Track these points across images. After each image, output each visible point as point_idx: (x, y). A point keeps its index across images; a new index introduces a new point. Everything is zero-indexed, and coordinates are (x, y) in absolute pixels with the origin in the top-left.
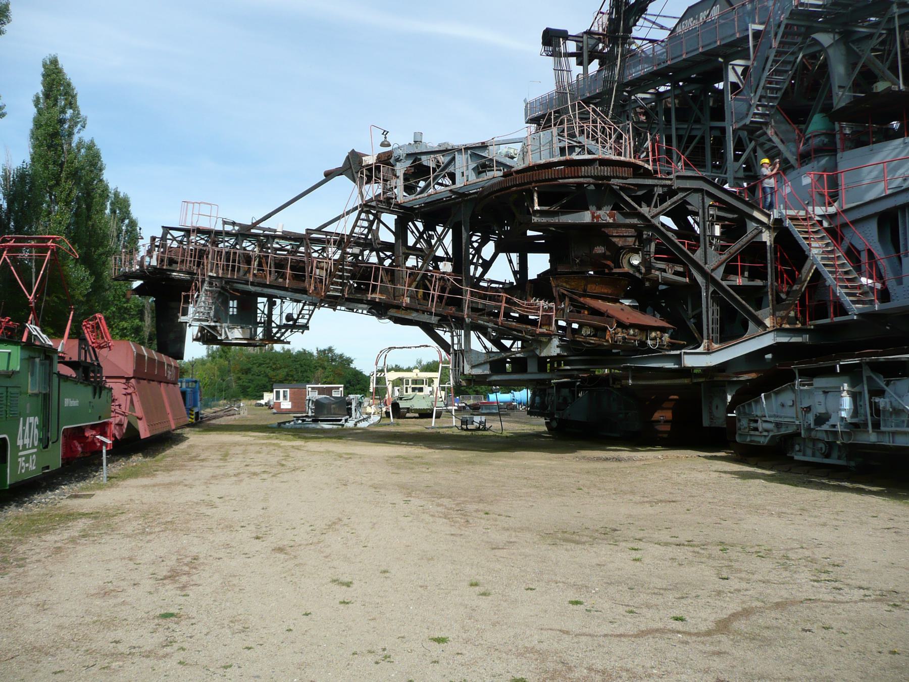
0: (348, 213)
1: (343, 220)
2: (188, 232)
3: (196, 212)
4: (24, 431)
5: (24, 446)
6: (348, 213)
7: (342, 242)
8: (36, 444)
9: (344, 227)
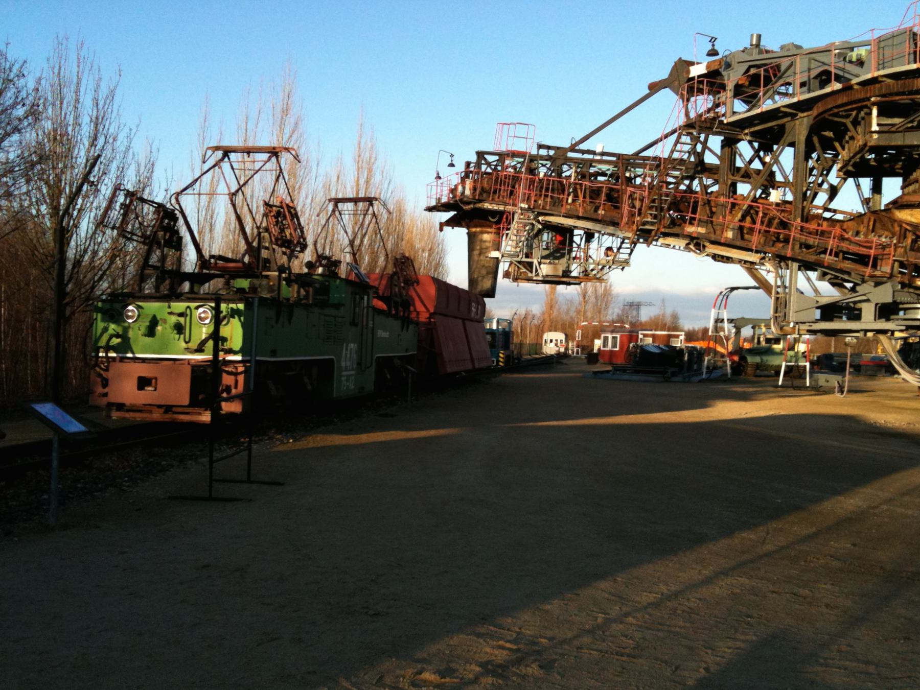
0: (666, 136)
1: (660, 144)
2: (502, 156)
3: (511, 134)
4: (346, 354)
5: (346, 367)
6: (666, 136)
7: (659, 164)
8: (355, 367)
9: (662, 151)
